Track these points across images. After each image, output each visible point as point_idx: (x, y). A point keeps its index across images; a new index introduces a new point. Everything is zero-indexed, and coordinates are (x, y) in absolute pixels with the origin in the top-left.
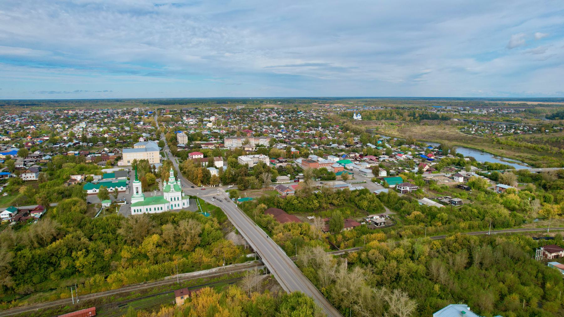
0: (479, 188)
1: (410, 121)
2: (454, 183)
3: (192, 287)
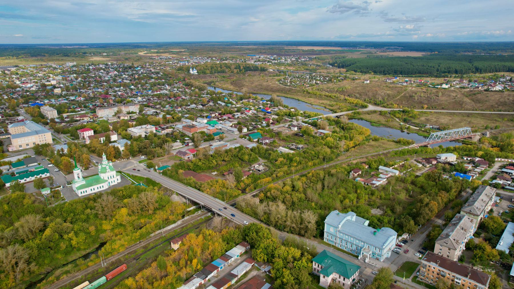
0: (309, 134)
1: (237, 73)
2: (292, 132)
3: (180, 235)
